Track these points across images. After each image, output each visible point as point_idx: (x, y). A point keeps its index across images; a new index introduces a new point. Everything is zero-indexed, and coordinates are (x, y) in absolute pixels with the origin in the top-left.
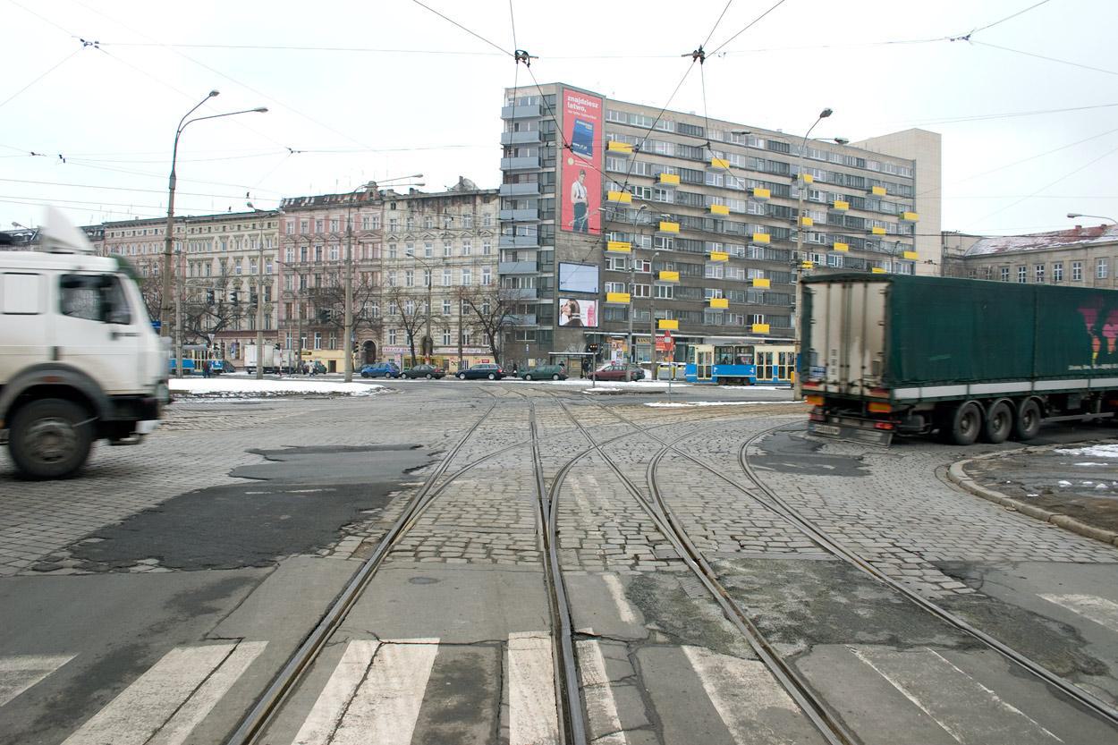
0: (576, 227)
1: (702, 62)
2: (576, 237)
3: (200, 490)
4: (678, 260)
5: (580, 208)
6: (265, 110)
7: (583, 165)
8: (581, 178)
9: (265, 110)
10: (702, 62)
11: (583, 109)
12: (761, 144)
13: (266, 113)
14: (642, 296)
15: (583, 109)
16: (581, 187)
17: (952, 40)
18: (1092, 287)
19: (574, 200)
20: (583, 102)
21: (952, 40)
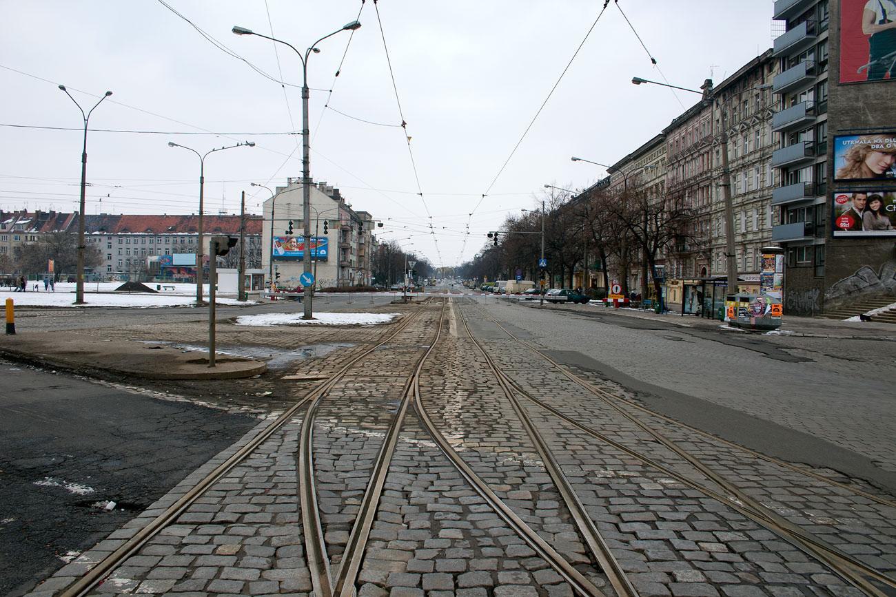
1: (709, 83)
19: (868, 29)
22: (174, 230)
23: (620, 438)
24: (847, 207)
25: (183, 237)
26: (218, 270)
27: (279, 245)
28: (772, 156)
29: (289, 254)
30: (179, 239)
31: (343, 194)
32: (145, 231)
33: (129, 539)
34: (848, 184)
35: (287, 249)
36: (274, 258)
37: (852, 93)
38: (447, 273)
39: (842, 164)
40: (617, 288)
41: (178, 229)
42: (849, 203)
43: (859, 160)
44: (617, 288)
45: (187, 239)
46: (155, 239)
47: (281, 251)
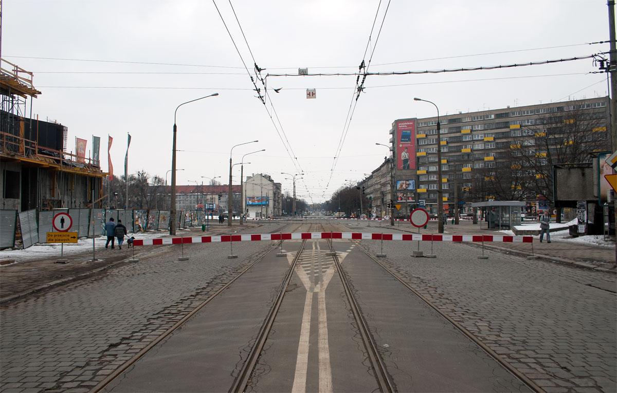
0: (404, 168)
1: (386, 157)
2: (404, 171)
3: (561, 223)
4: (450, 173)
5: (406, 161)
6: (217, 94)
7: (406, 145)
8: (406, 150)
9: (217, 94)
10: (386, 157)
11: (406, 126)
12: (493, 116)
13: (217, 96)
14: (526, 124)
15: (406, 126)
16: (406, 154)
17: (590, 44)
18: (327, 329)
19: (402, 159)
20: (406, 124)
21: (590, 44)
22: (193, 192)
23: (524, 366)
24: (400, 195)
25: (198, 195)
26: (541, 229)
27: (250, 200)
28: (187, 259)
29: (254, 203)
30: (196, 197)
31: (272, 178)
32: (181, 193)
33: (160, 335)
34: (400, 191)
35: (252, 201)
36: (247, 205)
37: (400, 171)
38: (316, 207)
39: (399, 186)
40: (63, 221)
41: (195, 192)
42: (400, 195)
43: (402, 186)
44: (63, 221)
45: (199, 197)
46: (185, 197)
47: (250, 203)
